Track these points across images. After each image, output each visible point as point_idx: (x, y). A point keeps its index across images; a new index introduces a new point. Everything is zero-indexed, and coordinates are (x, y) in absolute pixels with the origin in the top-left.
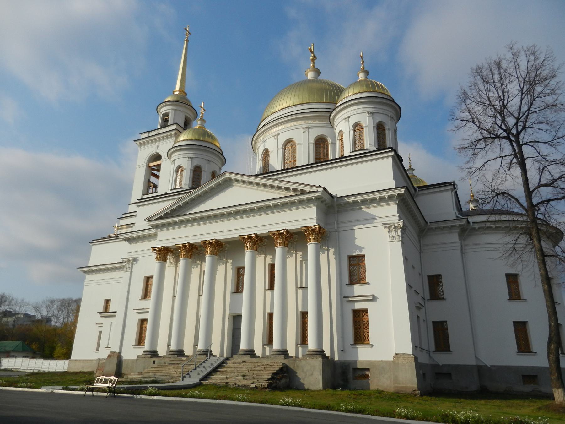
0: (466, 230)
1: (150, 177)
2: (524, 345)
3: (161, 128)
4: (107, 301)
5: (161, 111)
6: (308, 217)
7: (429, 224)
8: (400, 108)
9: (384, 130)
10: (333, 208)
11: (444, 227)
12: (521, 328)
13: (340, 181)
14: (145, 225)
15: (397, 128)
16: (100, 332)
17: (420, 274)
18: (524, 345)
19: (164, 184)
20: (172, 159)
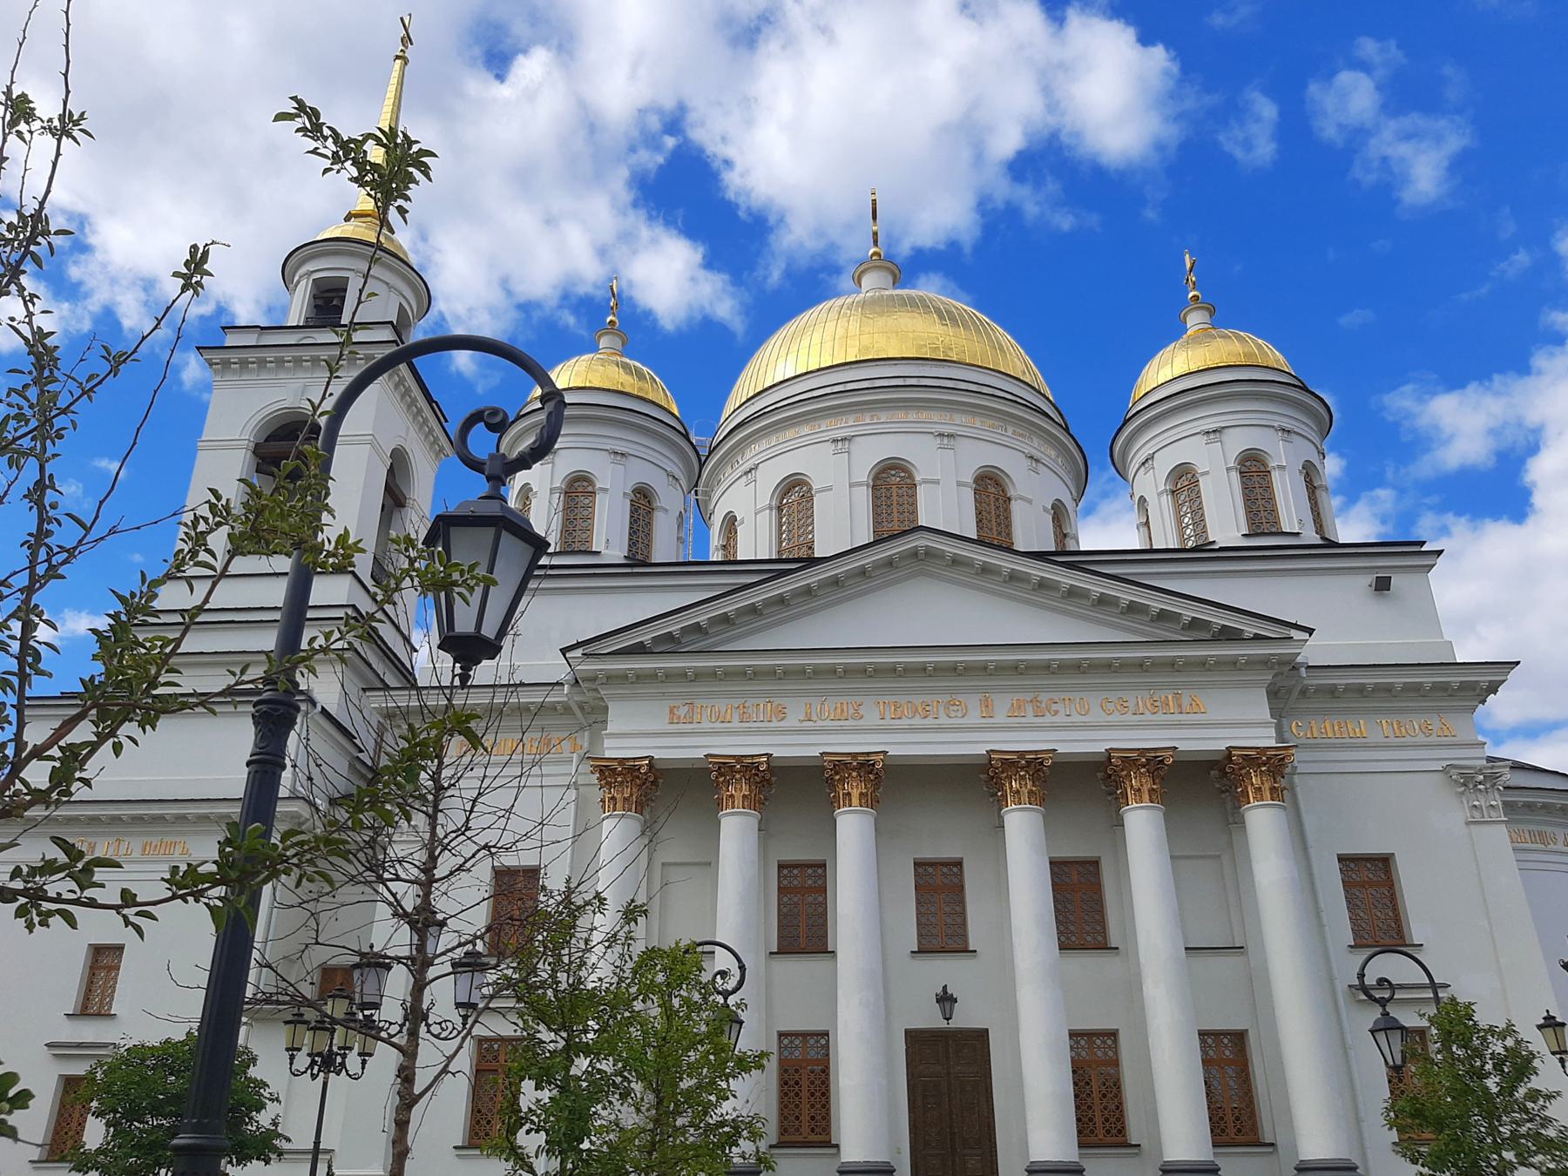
6: (1233, 721)
14: (557, 669)
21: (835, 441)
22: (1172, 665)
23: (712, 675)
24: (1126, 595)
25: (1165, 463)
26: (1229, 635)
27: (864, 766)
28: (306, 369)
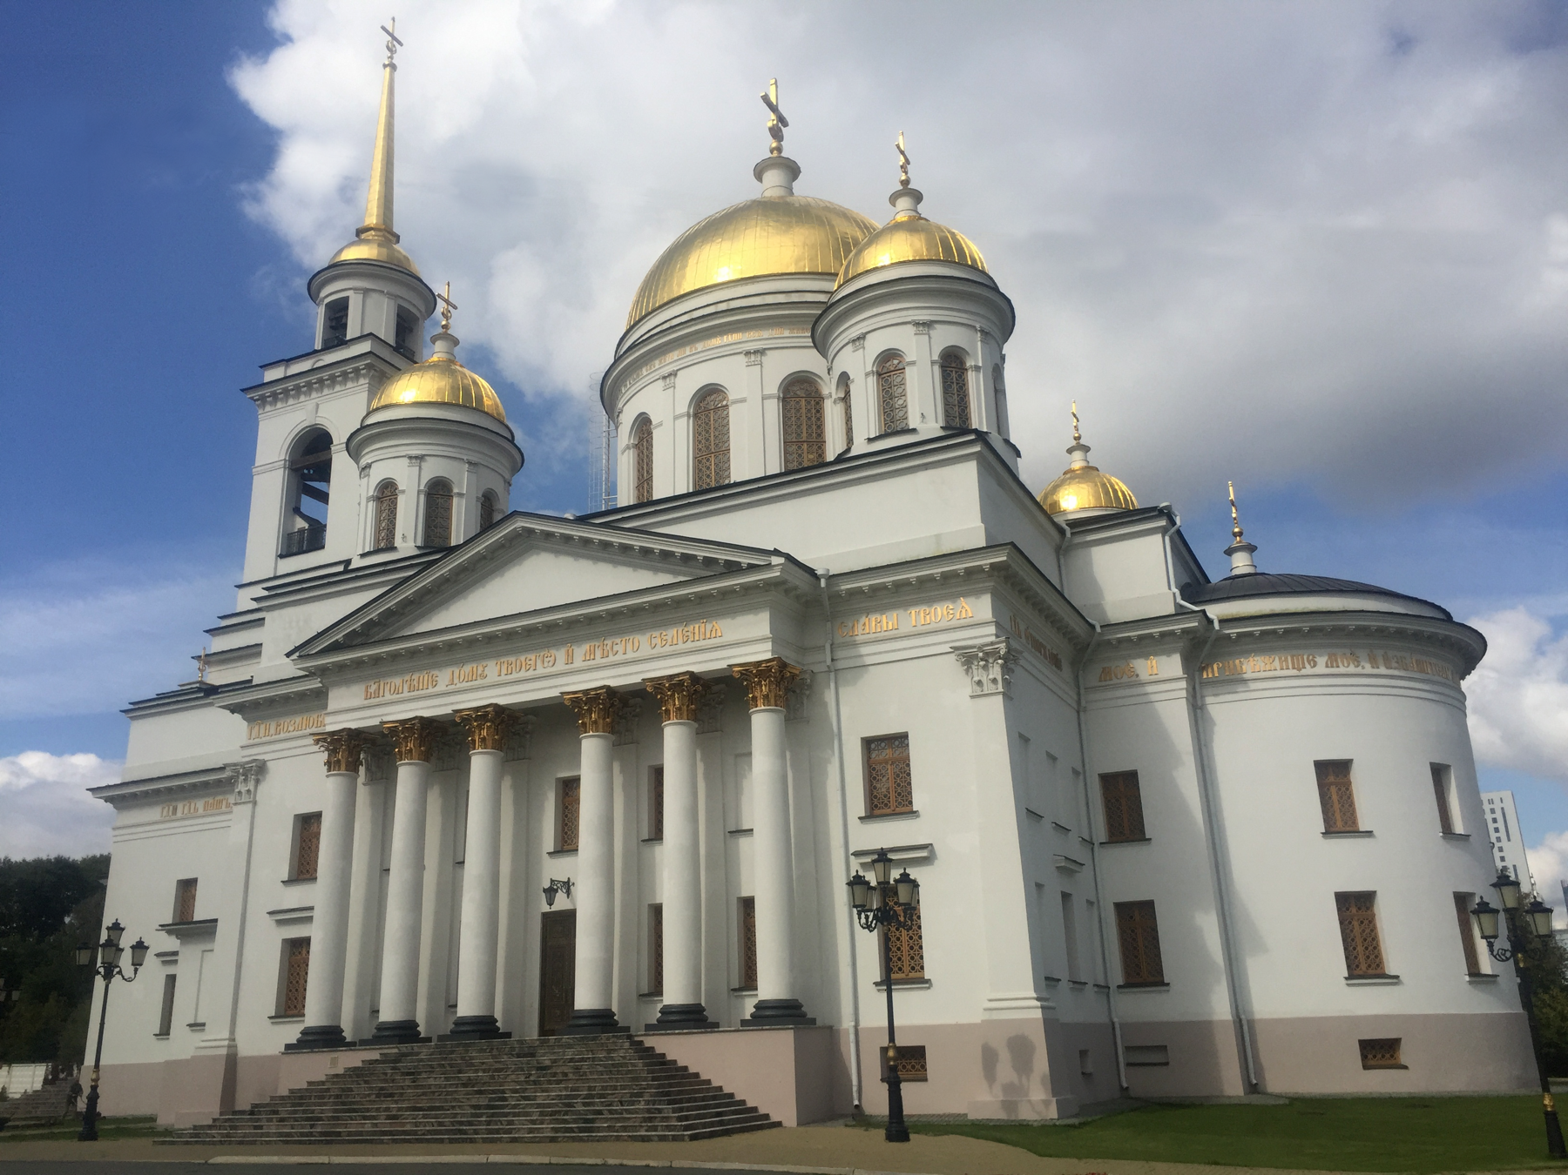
0: (1205, 642)
1: (298, 500)
2: (1364, 959)
3: (328, 346)
4: (187, 888)
5: (322, 295)
6: (744, 640)
7: (1098, 629)
8: (1008, 301)
9: (962, 370)
10: (820, 607)
11: (1144, 637)
12: (1356, 909)
13: (832, 531)
14: (289, 668)
15: (1003, 358)
16: (171, 980)
17: (1076, 772)
18: (1364, 959)
19: (348, 528)
20: (363, 462)
21: (748, 353)
22: (702, 598)
23: (395, 657)
24: (637, 542)
25: (877, 344)
26: (732, 568)
27: (675, 684)
28: (352, 380)
